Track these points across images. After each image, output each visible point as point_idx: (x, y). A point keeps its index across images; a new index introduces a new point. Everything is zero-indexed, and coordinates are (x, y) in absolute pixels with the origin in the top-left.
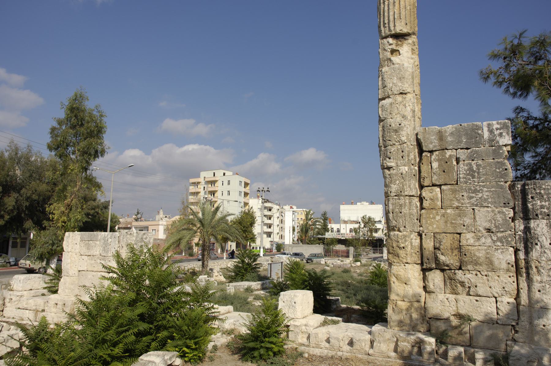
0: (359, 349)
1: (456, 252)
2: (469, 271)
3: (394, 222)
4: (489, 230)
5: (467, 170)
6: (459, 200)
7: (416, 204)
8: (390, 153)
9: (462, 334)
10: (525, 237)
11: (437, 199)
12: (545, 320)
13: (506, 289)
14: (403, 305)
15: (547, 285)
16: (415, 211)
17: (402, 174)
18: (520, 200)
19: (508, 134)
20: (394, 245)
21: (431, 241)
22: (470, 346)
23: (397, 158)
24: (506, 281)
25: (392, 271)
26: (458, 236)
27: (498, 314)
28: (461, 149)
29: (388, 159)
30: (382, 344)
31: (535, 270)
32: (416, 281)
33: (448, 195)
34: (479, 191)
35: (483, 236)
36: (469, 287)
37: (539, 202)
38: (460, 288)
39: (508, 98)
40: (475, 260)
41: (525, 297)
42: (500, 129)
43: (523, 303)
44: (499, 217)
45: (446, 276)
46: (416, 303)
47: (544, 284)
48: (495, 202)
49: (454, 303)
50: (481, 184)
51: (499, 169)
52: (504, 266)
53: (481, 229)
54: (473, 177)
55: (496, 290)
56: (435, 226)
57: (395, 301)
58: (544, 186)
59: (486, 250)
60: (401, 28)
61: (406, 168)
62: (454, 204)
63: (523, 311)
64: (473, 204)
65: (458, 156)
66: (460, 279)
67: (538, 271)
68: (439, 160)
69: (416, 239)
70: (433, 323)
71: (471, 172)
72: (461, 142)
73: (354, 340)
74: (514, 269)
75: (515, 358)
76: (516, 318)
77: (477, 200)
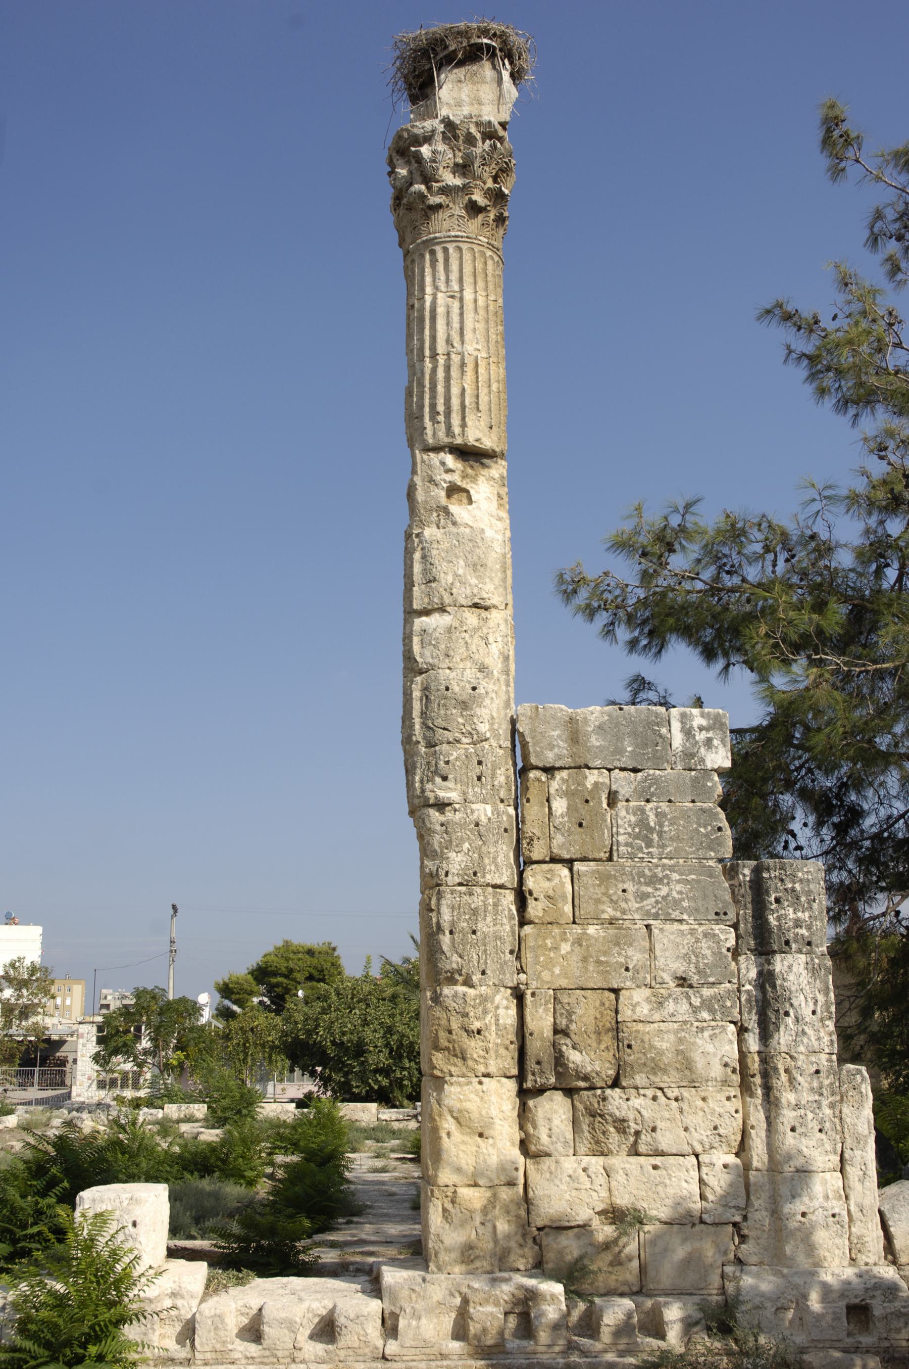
0: (356, 1345)
1: (608, 1040)
2: (637, 1088)
3: (455, 958)
4: (682, 981)
5: (636, 825)
6: (616, 902)
7: (510, 910)
8: (447, 763)
9: (620, 1264)
10: (760, 997)
11: (564, 897)
12: (806, 1199)
13: (721, 1131)
14: (474, 1197)
15: (808, 1113)
16: (508, 928)
17: (477, 825)
18: (749, 906)
20: (455, 1026)
21: (546, 1010)
22: (639, 1292)
23: (464, 778)
24: (722, 1110)
25: (446, 1102)
26: (613, 996)
27: (702, 1197)
28: (622, 769)
29: (438, 780)
30: (424, 1321)
31: (784, 1077)
33: (591, 888)
34: (661, 881)
35: (670, 995)
36: (637, 1133)
37: (791, 910)
38: (614, 1137)
39: (618, 651)
41: (760, 1147)
42: (707, 729)
43: (755, 1163)
44: (706, 948)
45: (580, 1106)
46: (504, 1188)
47: (803, 1111)
48: (697, 910)
49: (602, 1179)
50: (665, 861)
51: (705, 828)
52: (717, 1071)
53: (667, 978)
54: (649, 844)
55: (701, 1135)
56: (557, 971)
57: (452, 1189)
58: (800, 874)
59: (676, 1032)
61: (489, 808)
62: (603, 912)
63: (755, 1184)
64: (648, 913)
65: (614, 787)
66: (617, 1113)
67: (792, 1080)
68: (568, 794)
69: (507, 1008)
70: (548, 1240)
72: (620, 751)
73: (341, 1320)
74: (736, 1078)
75: (749, 1306)
76: (742, 1204)
77: (657, 902)
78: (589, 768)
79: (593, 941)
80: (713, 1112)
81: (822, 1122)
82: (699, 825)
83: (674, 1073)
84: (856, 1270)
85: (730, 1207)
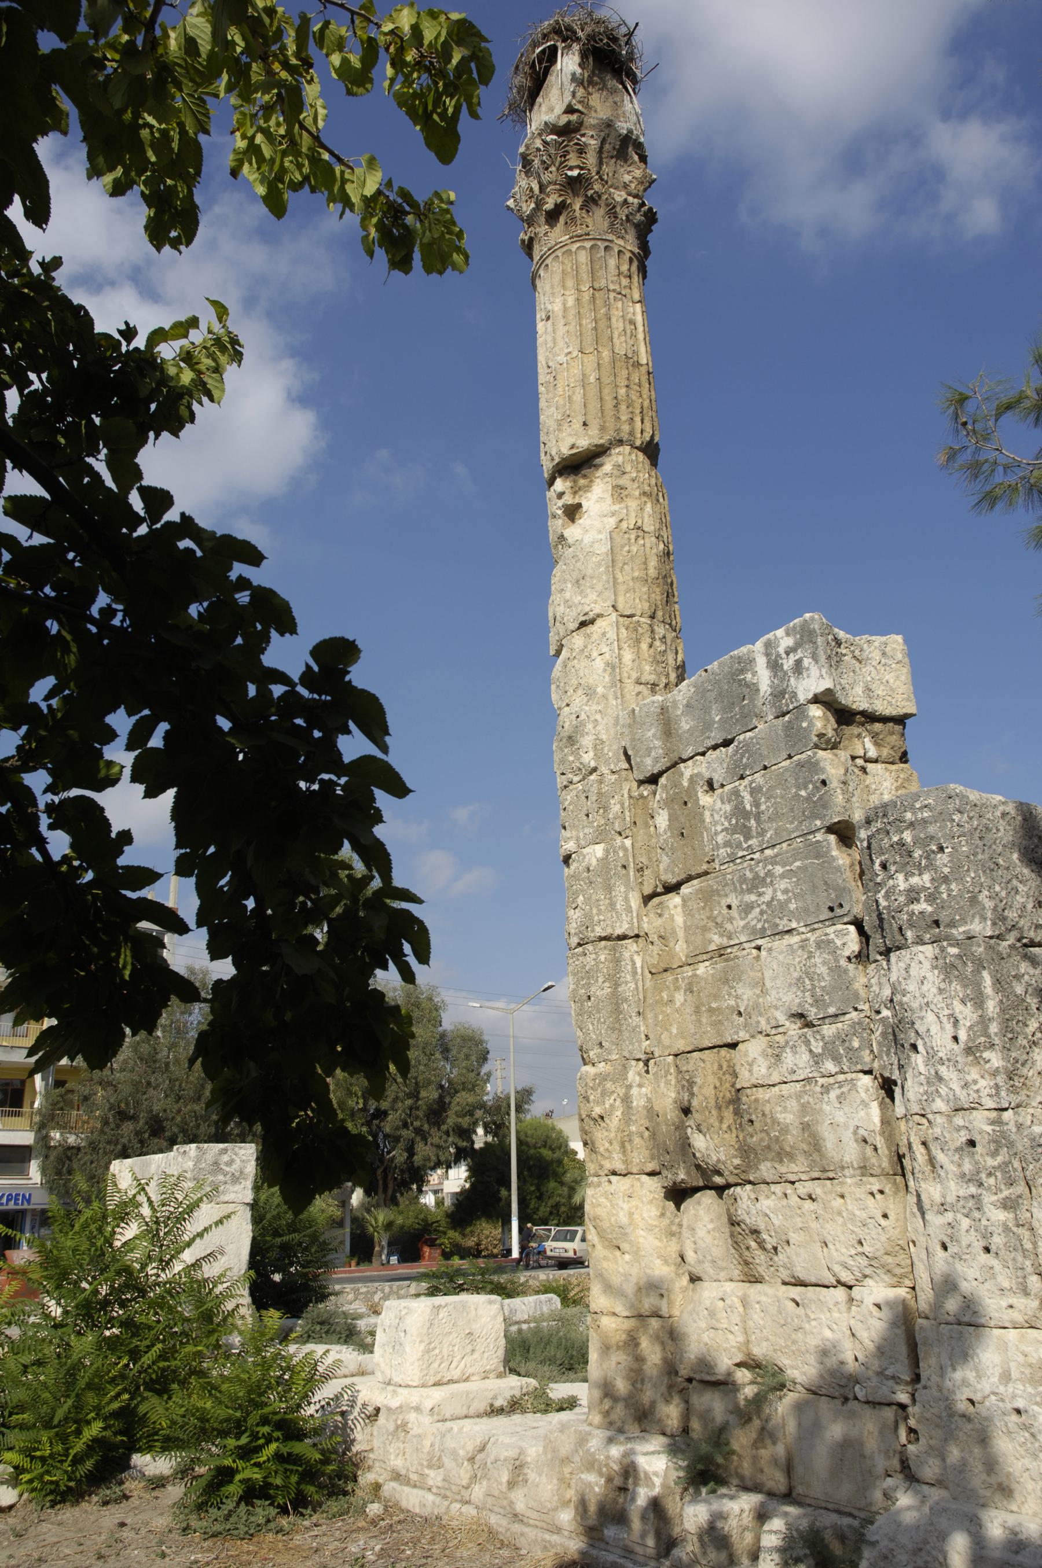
1: (728, 1115)
5: (733, 815)
16: (632, 986)
19: (815, 658)
21: (668, 1083)
24: (864, 1215)
28: (715, 747)
32: (651, 1238)
37: (900, 877)
40: (777, 1139)
44: (820, 964)
51: (806, 788)
52: (851, 1152)
53: (782, 1018)
58: (908, 816)
59: (798, 1096)
60: (571, 441)
64: (754, 931)
69: (640, 1086)
71: (742, 820)
77: (762, 913)
78: (684, 761)
79: (703, 984)
80: (853, 1218)
81: (987, 1235)
82: (799, 788)
83: (801, 1158)
84: (123, 1487)
85: (887, 1378)
